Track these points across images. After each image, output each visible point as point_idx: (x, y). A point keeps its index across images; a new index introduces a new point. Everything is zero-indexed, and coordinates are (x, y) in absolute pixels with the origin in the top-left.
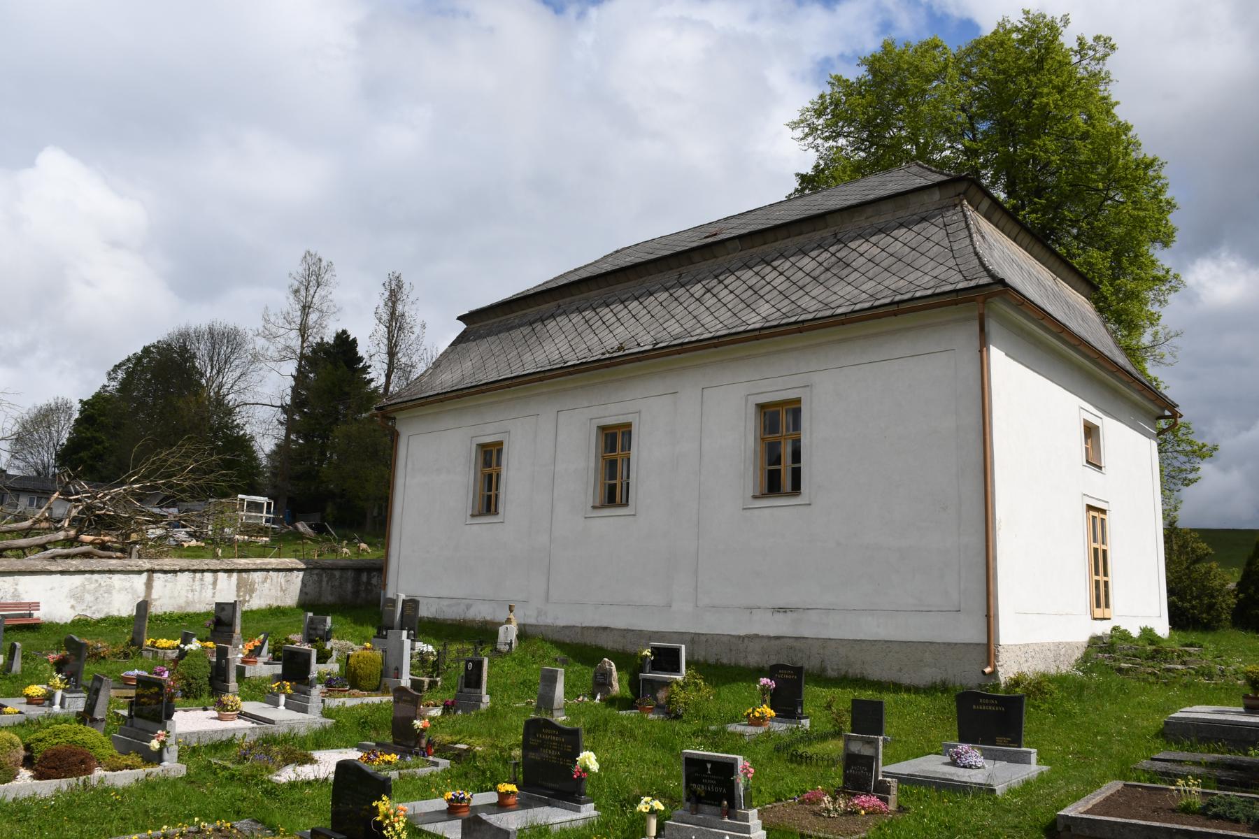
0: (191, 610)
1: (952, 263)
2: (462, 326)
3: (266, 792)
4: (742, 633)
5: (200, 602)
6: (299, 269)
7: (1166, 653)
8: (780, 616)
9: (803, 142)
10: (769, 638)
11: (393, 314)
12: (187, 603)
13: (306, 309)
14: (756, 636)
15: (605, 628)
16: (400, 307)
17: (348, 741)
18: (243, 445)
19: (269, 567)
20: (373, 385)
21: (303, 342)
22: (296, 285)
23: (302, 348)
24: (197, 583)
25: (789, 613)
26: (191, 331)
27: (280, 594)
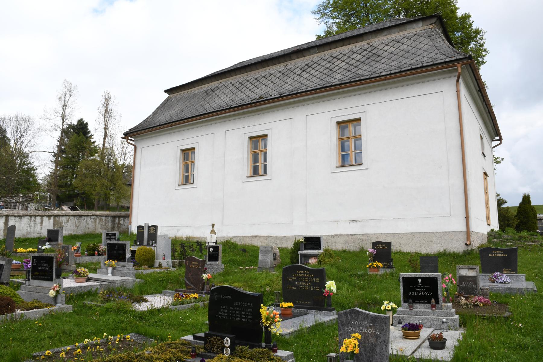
0: (29, 236)
1: (437, 52)
2: (166, 95)
3: (135, 316)
4: (333, 234)
5: (34, 232)
6: (62, 89)
7: (525, 238)
8: (354, 224)
9: (318, 21)
10: (348, 235)
11: (106, 110)
12: (27, 233)
13: (64, 106)
14: (341, 235)
15: (256, 236)
16: (109, 107)
17: (520, 212)
18: (29, 173)
19: (70, 214)
20: (96, 144)
21: (63, 122)
22: (59, 96)
23: (63, 125)
24: (32, 223)
25: (359, 223)
26: (6, 117)
27: (75, 228)
